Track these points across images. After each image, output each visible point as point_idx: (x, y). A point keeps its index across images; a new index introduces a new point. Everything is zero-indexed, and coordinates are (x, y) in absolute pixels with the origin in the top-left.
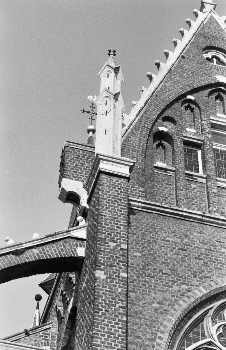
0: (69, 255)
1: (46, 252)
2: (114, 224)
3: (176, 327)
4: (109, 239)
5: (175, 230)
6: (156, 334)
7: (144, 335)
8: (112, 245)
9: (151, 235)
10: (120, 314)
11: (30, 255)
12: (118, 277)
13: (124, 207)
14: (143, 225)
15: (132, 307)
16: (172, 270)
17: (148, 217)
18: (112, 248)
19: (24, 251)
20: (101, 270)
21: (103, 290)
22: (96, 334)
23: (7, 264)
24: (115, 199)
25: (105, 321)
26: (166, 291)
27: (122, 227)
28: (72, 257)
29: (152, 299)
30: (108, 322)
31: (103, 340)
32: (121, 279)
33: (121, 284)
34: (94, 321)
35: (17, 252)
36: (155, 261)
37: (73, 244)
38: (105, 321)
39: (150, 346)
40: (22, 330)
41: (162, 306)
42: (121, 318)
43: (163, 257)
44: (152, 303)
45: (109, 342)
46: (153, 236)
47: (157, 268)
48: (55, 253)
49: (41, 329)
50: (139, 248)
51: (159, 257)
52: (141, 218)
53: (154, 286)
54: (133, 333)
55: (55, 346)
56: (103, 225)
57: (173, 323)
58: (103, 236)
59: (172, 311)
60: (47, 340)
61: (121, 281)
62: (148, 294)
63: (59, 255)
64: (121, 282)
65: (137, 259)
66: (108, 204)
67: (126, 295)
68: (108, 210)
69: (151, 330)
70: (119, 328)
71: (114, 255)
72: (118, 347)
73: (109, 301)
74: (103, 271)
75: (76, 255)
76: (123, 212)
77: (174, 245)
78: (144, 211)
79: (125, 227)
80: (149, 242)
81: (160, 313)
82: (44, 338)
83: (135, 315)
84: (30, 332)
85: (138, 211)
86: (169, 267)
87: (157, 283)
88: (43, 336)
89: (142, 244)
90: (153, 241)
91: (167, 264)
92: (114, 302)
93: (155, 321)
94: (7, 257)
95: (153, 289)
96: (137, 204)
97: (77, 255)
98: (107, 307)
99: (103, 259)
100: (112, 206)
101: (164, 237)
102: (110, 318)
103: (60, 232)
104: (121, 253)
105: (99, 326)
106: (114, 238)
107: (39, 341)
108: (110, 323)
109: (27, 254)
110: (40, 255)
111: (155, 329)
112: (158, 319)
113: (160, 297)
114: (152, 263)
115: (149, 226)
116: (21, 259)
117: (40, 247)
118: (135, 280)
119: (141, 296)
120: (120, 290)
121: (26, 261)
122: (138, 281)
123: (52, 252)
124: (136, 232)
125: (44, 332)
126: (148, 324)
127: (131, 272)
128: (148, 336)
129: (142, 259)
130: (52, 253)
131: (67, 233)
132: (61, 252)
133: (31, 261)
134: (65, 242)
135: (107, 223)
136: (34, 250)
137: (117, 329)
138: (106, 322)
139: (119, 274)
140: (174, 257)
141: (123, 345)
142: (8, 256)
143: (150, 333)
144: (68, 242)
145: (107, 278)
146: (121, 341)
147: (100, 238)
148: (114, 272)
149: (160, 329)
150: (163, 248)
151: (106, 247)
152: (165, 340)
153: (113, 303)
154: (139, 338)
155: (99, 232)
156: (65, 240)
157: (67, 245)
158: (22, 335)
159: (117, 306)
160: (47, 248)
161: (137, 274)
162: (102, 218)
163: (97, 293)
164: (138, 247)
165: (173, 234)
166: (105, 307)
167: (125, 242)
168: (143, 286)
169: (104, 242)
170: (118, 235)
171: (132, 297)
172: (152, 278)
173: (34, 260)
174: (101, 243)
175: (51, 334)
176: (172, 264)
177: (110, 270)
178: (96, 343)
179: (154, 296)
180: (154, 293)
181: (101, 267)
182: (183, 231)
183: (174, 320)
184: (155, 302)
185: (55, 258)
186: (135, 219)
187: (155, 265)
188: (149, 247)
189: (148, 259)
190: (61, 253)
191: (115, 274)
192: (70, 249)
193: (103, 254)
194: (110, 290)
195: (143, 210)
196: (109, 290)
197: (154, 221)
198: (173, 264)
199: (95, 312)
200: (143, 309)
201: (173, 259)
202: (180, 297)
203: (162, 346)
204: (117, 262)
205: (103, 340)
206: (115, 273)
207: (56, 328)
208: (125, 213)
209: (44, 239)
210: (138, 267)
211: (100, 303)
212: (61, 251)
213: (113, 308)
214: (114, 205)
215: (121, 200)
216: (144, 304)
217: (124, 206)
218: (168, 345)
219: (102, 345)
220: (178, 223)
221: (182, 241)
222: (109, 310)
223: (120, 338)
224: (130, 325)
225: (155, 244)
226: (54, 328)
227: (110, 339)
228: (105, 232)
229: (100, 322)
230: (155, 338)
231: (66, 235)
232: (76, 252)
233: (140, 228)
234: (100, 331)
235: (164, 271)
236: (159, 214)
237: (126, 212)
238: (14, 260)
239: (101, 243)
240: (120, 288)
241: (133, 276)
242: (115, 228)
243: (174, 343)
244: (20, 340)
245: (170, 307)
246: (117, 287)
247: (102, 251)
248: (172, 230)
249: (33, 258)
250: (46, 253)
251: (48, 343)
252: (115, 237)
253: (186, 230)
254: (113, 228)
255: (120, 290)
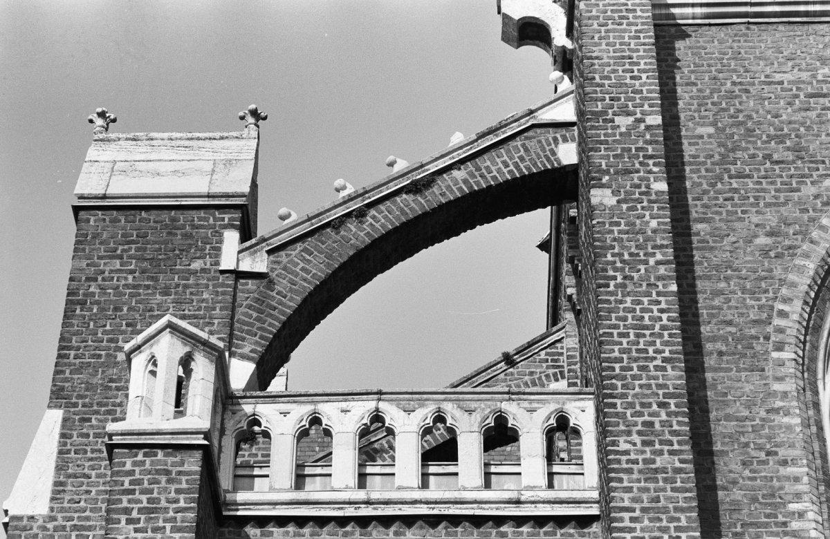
0: (540, 166)
1: (484, 171)
2: (623, 71)
3: (819, 282)
4: (614, 111)
5: (794, 52)
6: (772, 308)
7: (740, 315)
8: (623, 122)
9: (735, 77)
10: (659, 278)
11: (448, 187)
12: (647, 193)
13: (643, 27)
14: (711, 59)
15: (704, 258)
16: (797, 149)
17: (723, 35)
18: (623, 130)
19: (433, 181)
20: (602, 186)
21: (612, 231)
22: (606, 335)
23: (397, 218)
24: (621, 11)
25: (626, 302)
26: (785, 204)
27: (644, 76)
28: (547, 171)
29: (753, 227)
30: (633, 302)
31: (625, 345)
32: (653, 197)
33: (656, 209)
34: (599, 306)
35: (416, 185)
36: (751, 137)
37: (547, 140)
38: (626, 302)
39: (759, 338)
40: (498, 356)
41: (779, 239)
42: (663, 288)
43: (771, 124)
44: (753, 237)
45: (641, 346)
46: (739, 80)
47: (757, 152)
48: (505, 171)
49: (542, 345)
50: (707, 116)
51: (759, 126)
52: (704, 42)
53: (754, 197)
54: (712, 316)
55: (577, 378)
56: (598, 80)
57: (812, 273)
58: (600, 106)
59: (804, 247)
60: (559, 367)
61: (655, 202)
62: (741, 220)
63: (516, 171)
64: (655, 206)
65: (704, 143)
66: (603, 29)
67: (669, 233)
68: (604, 42)
69: (759, 299)
70: (662, 311)
71: (630, 146)
72: (663, 355)
73: (631, 254)
74: (608, 188)
75: (555, 163)
76: (642, 40)
77: (794, 89)
78: (710, 25)
79: (650, 74)
80: (731, 95)
81: (776, 257)
82: (550, 364)
83: (714, 273)
84: (515, 357)
85: (695, 28)
86: (788, 143)
87: (762, 189)
88: (547, 361)
89: (713, 104)
90: (739, 90)
91: (781, 139)
92: (641, 254)
93: (766, 278)
94: (395, 203)
95: (752, 205)
96: (689, 11)
97: (559, 163)
98: (627, 269)
99: (606, 161)
100: (614, 31)
101: (767, 76)
102: (636, 294)
103: (512, 119)
104: (648, 137)
105: (613, 315)
106: (627, 106)
107: (540, 373)
108: (638, 304)
109: (440, 187)
110: (471, 181)
111: (766, 295)
112: (771, 270)
113: (771, 218)
114: (744, 144)
115: (727, 57)
116: (429, 201)
117: (469, 163)
118: (705, 192)
119: (725, 227)
120: (654, 224)
121: (441, 202)
122: (712, 193)
123: (500, 168)
124: (696, 79)
125: (548, 350)
126: (748, 287)
127: (694, 175)
128: (752, 316)
129: (717, 140)
130: (499, 171)
131: (527, 118)
132: (520, 164)
133: (452, 198)
134: (526, 138)
135: (606, 74)
136: (455, 173)
137: (656, 313)
138: (628, 305)
139: (648, 187)
140: (798, 117)
141: (674, 348)
142: (398, 199)
143: (756, 307)
144: (534, 138)
145: (618, 202)
146: (669, 341)
147: (593, 113)
148: (635, 184)
149: (779, 295)
150: (766, 103)
151: (610, 131)
152: (795, 317)
153: (640, 256)
154: (730, 323)
155: (589, 100)
156: (526, 134)
157: (531, 144)
158: (499, 366)
159: (652, 261)
160: (485, 161)
161: (708, 178)
162: (593, 65)
163: (598, 241)
164: (703, 113)
165: (790, 64)
166: (622, 270)
167: (654, 109)
168: (726, 202)
169: (605, 121)
170: (635, 95)
171: (702, 233)
172: (746, 180)
173: (460, 196)
174: (597, 124)
175: (565, 353)
176: (793, 136)
177: (625, 182)
178: (611, 355)
179: (755, 219)
180: (756, 212)
181: (601, 179)
182: (814, 50)
183: (812, 266)
184: (761, 233)
185: (507, 182)
186: (690, 48)
187: (750, 146)
188: (732, 108)
189: (732, 135)
190: (519, 166)
191: (637, 190)
192: (541, 153)
193: (605, 149)
194: (629, 230)
195: (707, 21)
196: (627, 228)
197: (739, 41)
198: (797, 136)
199: (600, 286)
200: (731, 256)
201: (795, 122)
202: (821, 210)
203: (788, 331)
204: (641, 159)
205: (625, 345)
206: (639, 186)
207: (575, 336)
208: (647, 40)
209: (476, 144)
210: (709, 161)
211: (608, 263)
212: (519, 161)
213: (642, 267)
214: (618, 27)
215: (635, 11)
216: (735, 243)
217: (643, 24)
218: (804, 327)
219: (625, 356)
220: (799, 33)
221: (814, 76)
222: (632, 274)
223: (666, 333)
224: (705, 299)
225: (747, 97)
226: (571, 336)
227: (641, 340)
228: (605, 97)
229: (613, 305)
230: (770, 317)
231: (528, 121)
232: (557, 157)
233: (705, 68)
234: (616, 327)
235: (776, 157)
236: (749, 23)
237: (650, 37)
238: (413, 205)
239: (597, 124)
240: (654, 218)
241: (700, 184)
242: (628, 81)
243: (822, 320)
244: (496, 378)
245: (799, 237)
246: (647, 218)
247: (601, 143)
248: (785, 54)
249: (456, 191)
250: (486, 174)
251: (562, 373)
252: (630, 103)
253: (821, 46)
254: (622, 82)
255: (654, 224)
